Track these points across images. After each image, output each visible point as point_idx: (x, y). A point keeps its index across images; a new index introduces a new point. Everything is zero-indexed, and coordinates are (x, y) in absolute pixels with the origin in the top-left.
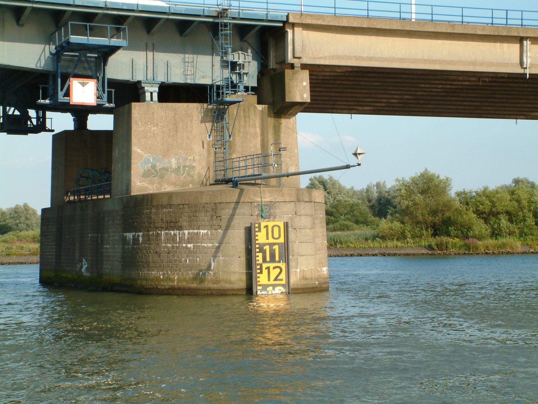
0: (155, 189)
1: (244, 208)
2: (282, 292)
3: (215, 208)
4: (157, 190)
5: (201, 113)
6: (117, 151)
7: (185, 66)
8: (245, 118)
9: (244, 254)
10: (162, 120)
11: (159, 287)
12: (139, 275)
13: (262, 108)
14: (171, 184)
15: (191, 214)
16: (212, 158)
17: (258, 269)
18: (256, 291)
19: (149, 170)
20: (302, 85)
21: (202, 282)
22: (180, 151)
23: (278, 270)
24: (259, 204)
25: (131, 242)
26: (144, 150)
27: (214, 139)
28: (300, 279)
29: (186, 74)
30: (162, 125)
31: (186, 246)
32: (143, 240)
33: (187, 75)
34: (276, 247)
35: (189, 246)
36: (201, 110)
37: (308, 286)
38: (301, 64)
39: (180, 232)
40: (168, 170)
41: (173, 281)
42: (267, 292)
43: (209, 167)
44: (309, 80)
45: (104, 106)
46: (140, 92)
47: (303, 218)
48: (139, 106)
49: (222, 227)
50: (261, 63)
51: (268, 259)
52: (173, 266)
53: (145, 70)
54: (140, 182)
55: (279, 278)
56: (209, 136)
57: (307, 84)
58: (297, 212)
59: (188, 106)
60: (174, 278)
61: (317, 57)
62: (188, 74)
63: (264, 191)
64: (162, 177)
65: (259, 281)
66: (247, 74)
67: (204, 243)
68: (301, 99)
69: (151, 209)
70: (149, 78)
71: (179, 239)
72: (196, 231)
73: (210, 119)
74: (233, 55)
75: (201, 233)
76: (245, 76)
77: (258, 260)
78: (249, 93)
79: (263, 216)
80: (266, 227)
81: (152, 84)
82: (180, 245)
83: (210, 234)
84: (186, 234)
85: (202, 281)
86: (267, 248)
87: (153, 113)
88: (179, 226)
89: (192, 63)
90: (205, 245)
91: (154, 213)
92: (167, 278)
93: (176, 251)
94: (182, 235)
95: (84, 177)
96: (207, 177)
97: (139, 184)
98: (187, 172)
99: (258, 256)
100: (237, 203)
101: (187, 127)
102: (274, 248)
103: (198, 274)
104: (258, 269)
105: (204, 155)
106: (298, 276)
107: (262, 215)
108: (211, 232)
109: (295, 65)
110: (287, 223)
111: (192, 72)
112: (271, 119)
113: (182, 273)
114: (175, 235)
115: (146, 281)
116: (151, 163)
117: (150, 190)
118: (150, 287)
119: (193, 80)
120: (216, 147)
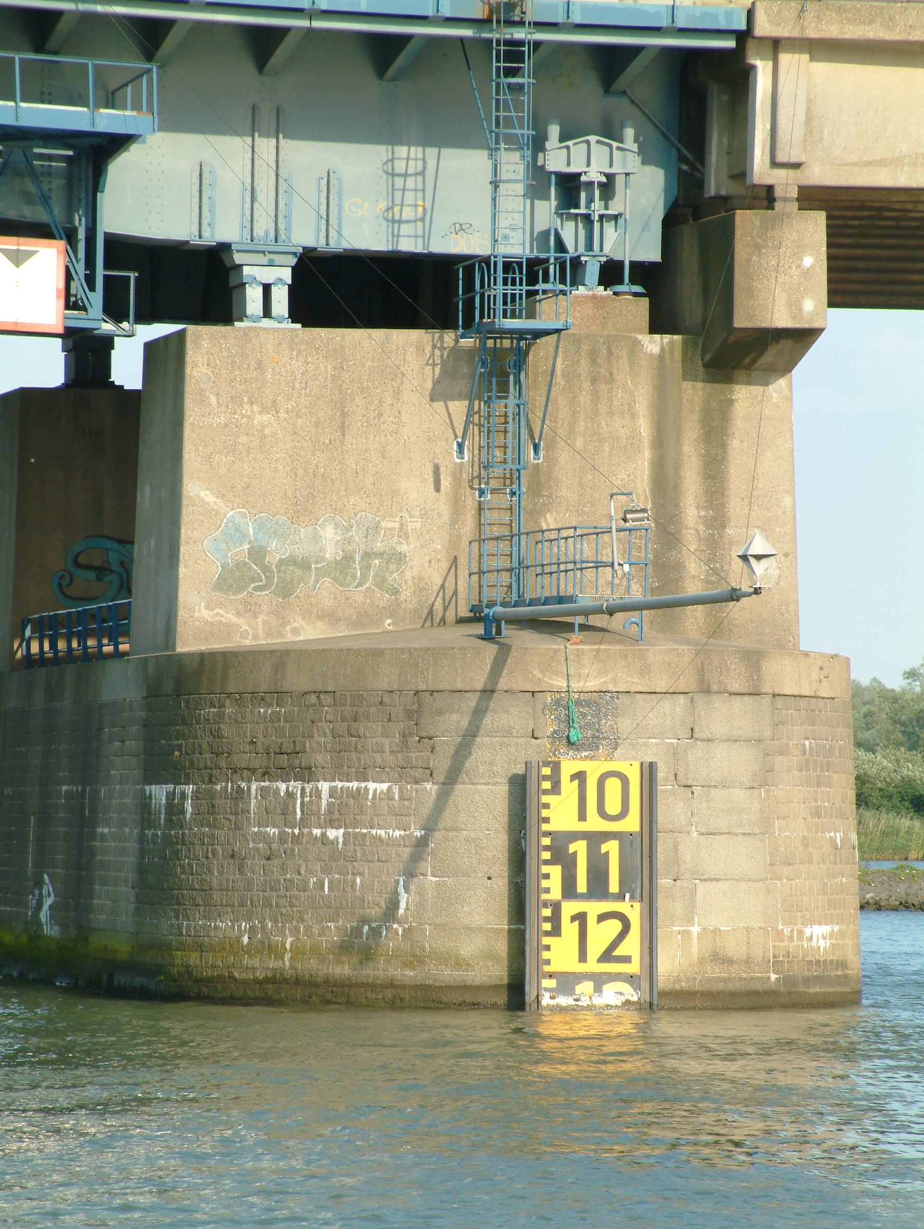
0: (260, 631)
1: (507, 712)
2: (627, 1003)
3: (415, 707)
4: (268, 634)
5: (434, 365)
6: (147, 488)
7: (393, 189)
8: (594, 381)
9: (505, 867)
10: (293, 388)
11: (237, 975)
12: (181, 934)
13: (662, 344)
14: (320, 617)
15: (342, 728)
16: (468, 527)
17: (547, 919)
18: (538, 996)
19: (241, 566)
20: (799, 266)
21: (367, 959)
22: (353, 500)
23: (615, 926)
24: (561, 699)
25: (163, 816)
26: (224, 495)
27: (476, 460)
28: (702, 961)
29: (397, 217)
30: (293, 408)
31: (324, 835)
32: (196, 813)
33: (400, 222)
34: (612, 848)
35: (332, 834)
36: (433, 354)
37: (731, 987)
38: (800, 187)
39: (306, 785)
40: (309, 568)
41: (275, 951)
42: (576, 1000)
43: (455, 558)
44: (825, 249)
45: (95, 332)
46: (233, 282)
47: (720, 751)
48: (212, 337)
49: (435, 774)
50: (680, 171)
51: (582, 886)
52: (282, 901)
53: (248, 205)
54: (207, 608)
55: (617, 952)
56: (460, 446)
57: (816, 261)
58: (696, 729)
59: (387, 338)
60: (283, 944)
61: (866, 158)
62: (404, 217)
63: (578, 656)
64: (285, 590)
65: (548, 962)
66: (616, 218)
67: (380, 827)
68: (794, 318)
69: (222, 706)
70: (259, 232)
71: (302, 811)
72: (354, 785)
73: (462, 385)
74: (568, 148)
75: (371, 792)
76: (609, 227)
77: (547, 891)
78: (619, 288)
79: (573, 739)
80: (580, 777)
81: (270, 258)
82: (306, 831)
83: (397, 797)
84: (325, 795)
85: (367, 955)
86: (579, 848)
87: (260, 363)
88: (303, 765)
89: (420, 178)
90: (382, 833)
91: (230, 717)
92: (262, 942)
93: (292, 850)
94: (311, 796)
95: (88, 567)
96: (449, 592)
97: (206, 614)
98: (376, 575)
99: (547, 876)
100: (488, 692)
101: (380, 415)
102: (603, 851)
103: (357, 931)
104: (547, 919)
105: (439, 516)
106: (695, 950)
107: (568, 737)
108: (401, 791)
109: (778, 192)
110: (651, 765)
111: (420, 209)
112: (694, 388)
113: (308, 929)
114: (290, 795)
115: (198, 954)
116: (250, 542)
117: (241, 637)
118: (210, 973)
119: (420, 240)
120: (483, 486)
